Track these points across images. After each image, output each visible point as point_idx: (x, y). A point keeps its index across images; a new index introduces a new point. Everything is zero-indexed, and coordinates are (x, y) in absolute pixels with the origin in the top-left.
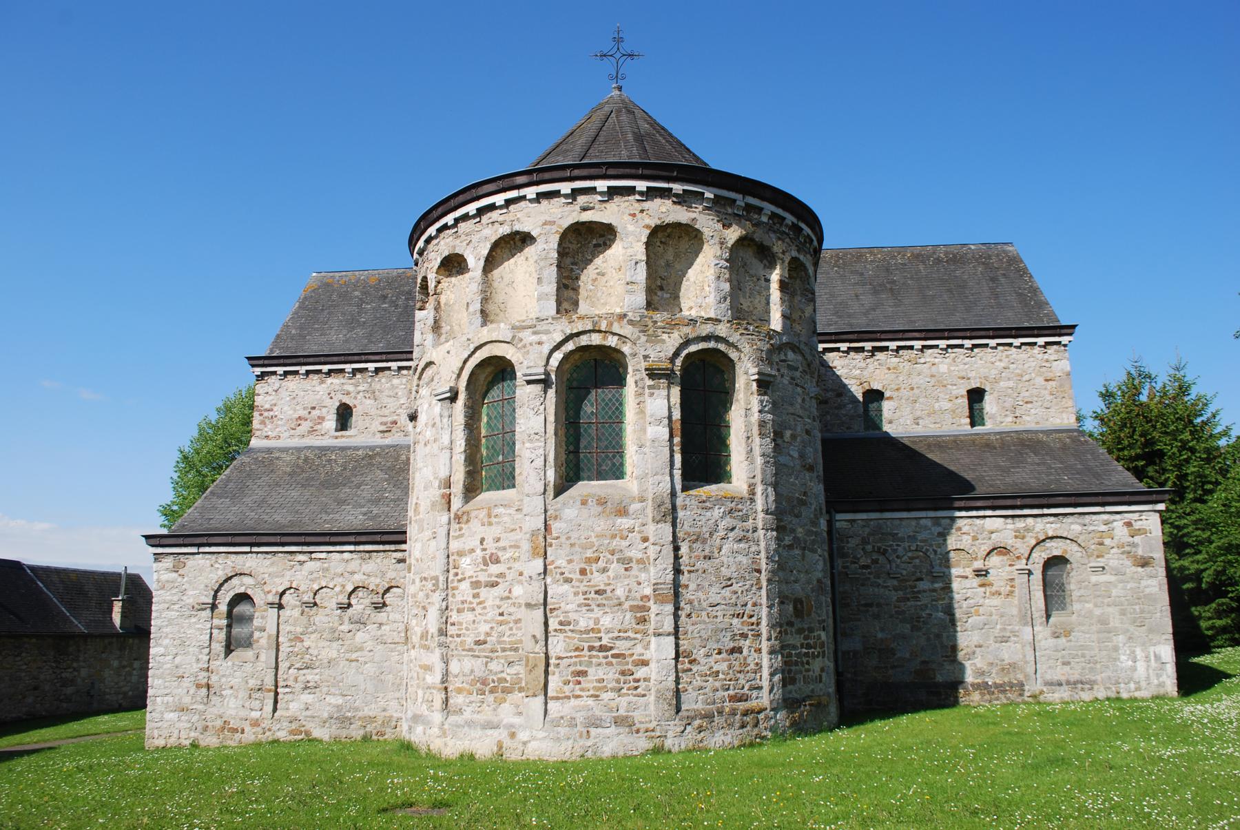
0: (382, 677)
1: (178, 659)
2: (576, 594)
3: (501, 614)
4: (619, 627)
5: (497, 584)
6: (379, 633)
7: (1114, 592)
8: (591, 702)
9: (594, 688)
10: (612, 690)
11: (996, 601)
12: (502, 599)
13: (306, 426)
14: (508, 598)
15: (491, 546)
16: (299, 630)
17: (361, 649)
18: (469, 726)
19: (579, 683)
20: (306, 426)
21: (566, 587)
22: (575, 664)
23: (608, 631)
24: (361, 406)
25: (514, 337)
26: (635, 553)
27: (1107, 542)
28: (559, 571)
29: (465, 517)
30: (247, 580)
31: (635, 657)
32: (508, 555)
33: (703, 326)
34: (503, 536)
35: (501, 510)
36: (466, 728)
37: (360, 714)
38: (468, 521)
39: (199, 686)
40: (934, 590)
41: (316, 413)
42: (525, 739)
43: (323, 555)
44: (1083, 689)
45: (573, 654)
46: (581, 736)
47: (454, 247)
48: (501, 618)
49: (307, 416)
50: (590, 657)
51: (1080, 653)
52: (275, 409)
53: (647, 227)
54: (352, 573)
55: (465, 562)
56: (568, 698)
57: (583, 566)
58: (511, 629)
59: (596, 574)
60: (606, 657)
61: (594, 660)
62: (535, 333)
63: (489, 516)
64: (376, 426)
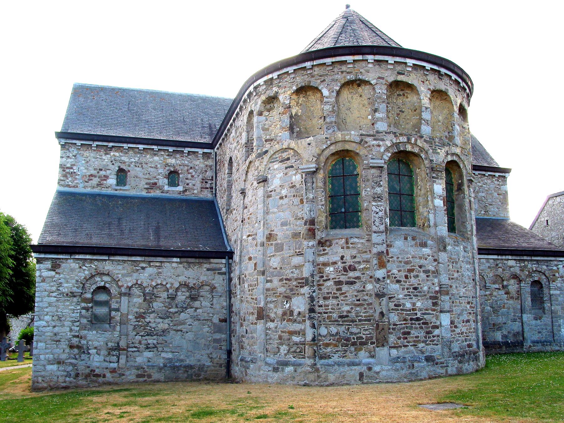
0: (198, 341)
1: (56, 329)
2: (403, 289)
3: (359, 300)
4: (425, 308)
5: (355, 282)
6: (195, 314)
7: (560, 299)
8: (412, 348)
9: (414, 341)
10: (423, 342)
11: (511, 302)
12: (358, 291)
13: (95, 181)
14: (363, 291)
15: (349, 261)
16: (142, 310)
17: (184, 323)
18: (339, 365)
19: (406, 338)
20: (95, 181)
21: (398, 285)
22: (404, 328)
23: (420, 310)
24: (134, 171)
25: (362, 140)
26: (431, 268)
27: (557, 275)
28: (394, 276)
29: (328, 243)
30: (106, 278)
31: (433, 324)
32: (362, 267)
33: (453, 148)
34: (358, 255)
35: (356, 240)
36: (336, 366)
37: (184, 364)
38: (330, 246)
39: (71, 347)
40: (486, 295)
41: (102, 173)
42: (378, 370)
43: (158, 264)
44: (547, 345)
45: (403, 322)
46: (409, 368)
47: (310, 82)
48: (358, 302)
49: (96, 174)
50: (412, 324)
51: (545, 327)
52: (75, 168)
53: (429, 89)
54: (178, 276)
55: (330, 269)
56: (401, 347)
57: (406, 273)
58: (365, 309)
59: (413, 278)
60: (419, 324)
61: (414, 326)
62: (375, 140)
63: (347, 243)
64: (143, 184)
